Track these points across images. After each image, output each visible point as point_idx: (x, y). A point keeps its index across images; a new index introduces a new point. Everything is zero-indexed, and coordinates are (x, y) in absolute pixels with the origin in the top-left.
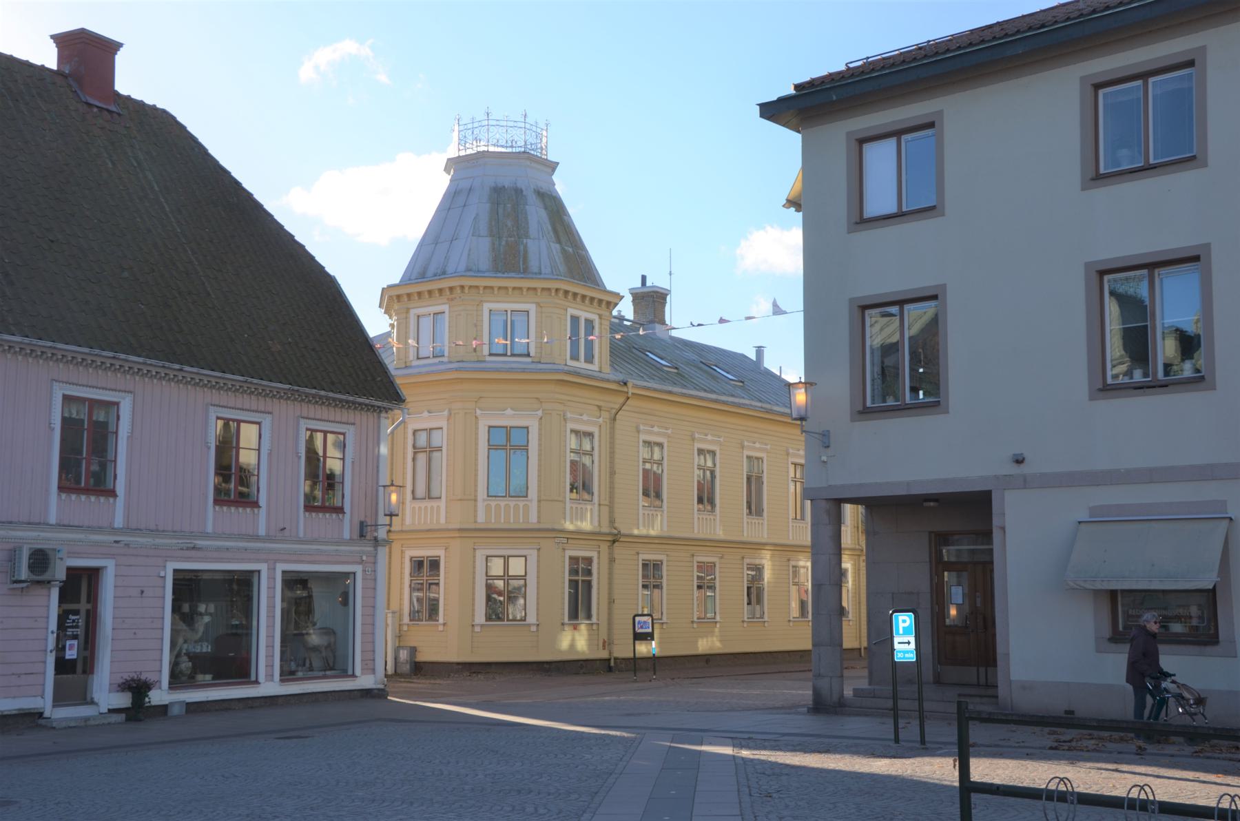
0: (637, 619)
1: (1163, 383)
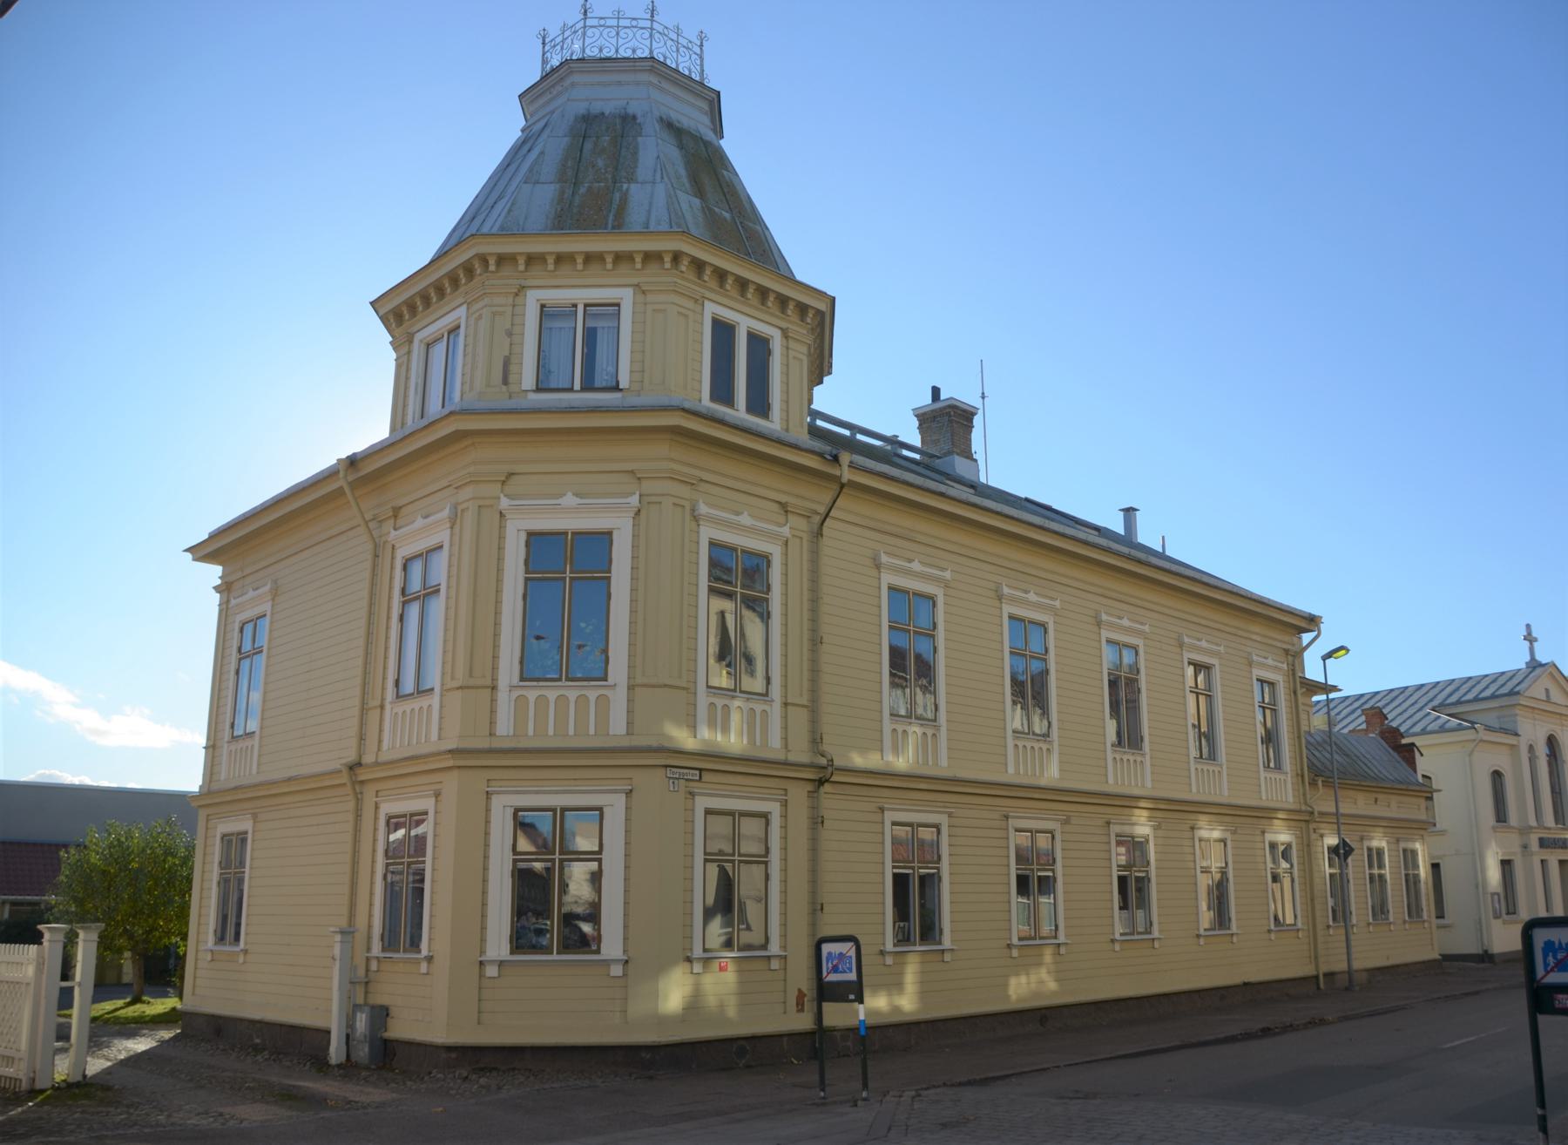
0: (827, 948)
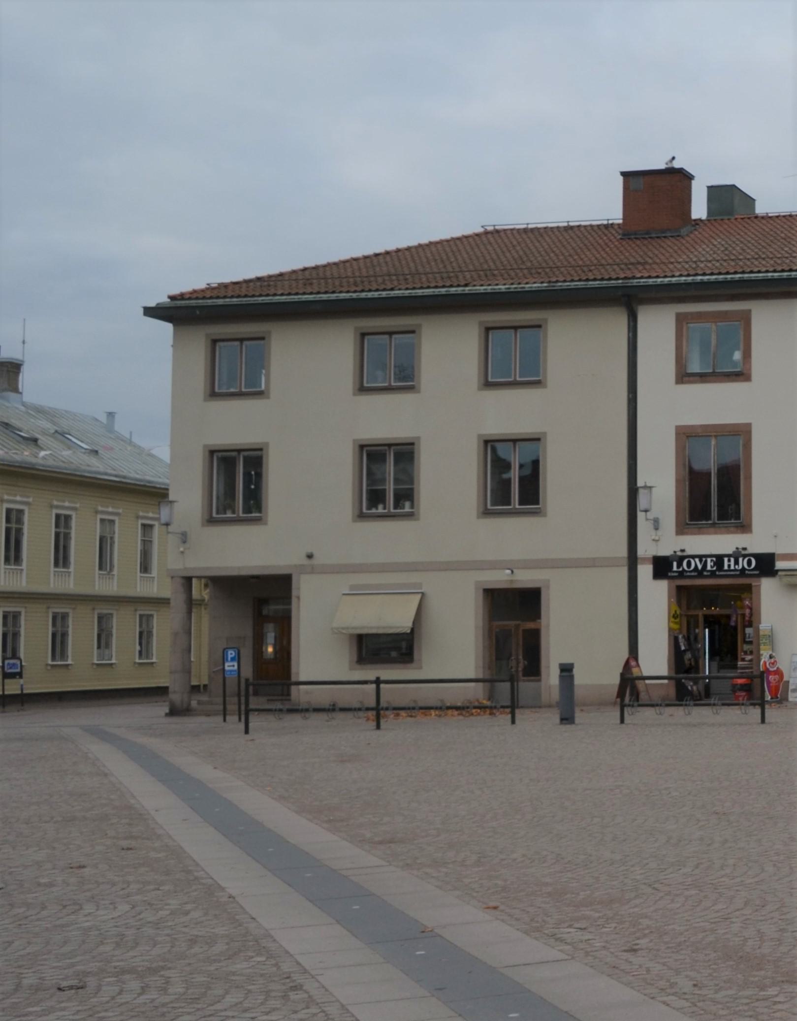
1: (393, 514)
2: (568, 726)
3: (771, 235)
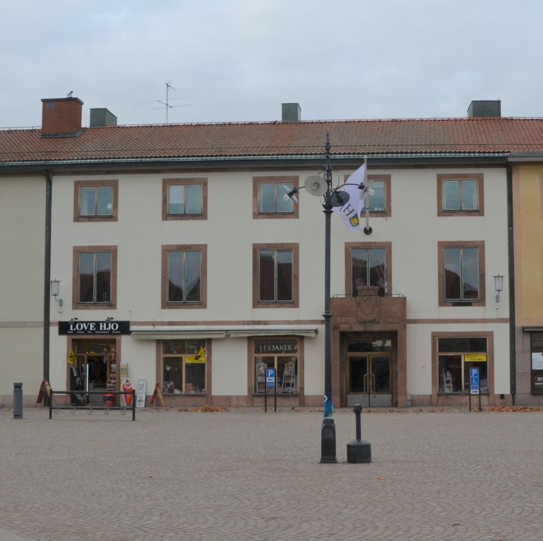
2: (19, 420)
3: (128, 138)
